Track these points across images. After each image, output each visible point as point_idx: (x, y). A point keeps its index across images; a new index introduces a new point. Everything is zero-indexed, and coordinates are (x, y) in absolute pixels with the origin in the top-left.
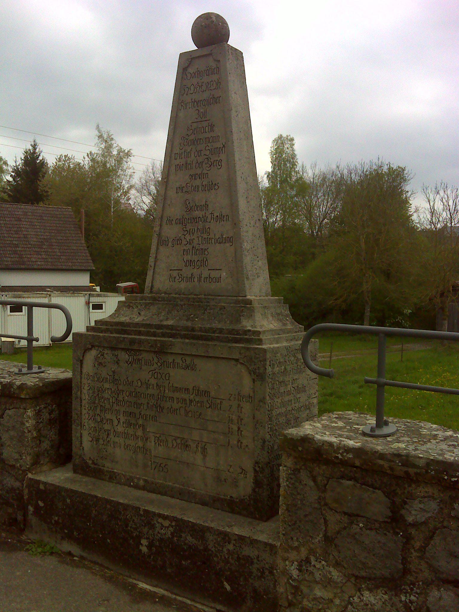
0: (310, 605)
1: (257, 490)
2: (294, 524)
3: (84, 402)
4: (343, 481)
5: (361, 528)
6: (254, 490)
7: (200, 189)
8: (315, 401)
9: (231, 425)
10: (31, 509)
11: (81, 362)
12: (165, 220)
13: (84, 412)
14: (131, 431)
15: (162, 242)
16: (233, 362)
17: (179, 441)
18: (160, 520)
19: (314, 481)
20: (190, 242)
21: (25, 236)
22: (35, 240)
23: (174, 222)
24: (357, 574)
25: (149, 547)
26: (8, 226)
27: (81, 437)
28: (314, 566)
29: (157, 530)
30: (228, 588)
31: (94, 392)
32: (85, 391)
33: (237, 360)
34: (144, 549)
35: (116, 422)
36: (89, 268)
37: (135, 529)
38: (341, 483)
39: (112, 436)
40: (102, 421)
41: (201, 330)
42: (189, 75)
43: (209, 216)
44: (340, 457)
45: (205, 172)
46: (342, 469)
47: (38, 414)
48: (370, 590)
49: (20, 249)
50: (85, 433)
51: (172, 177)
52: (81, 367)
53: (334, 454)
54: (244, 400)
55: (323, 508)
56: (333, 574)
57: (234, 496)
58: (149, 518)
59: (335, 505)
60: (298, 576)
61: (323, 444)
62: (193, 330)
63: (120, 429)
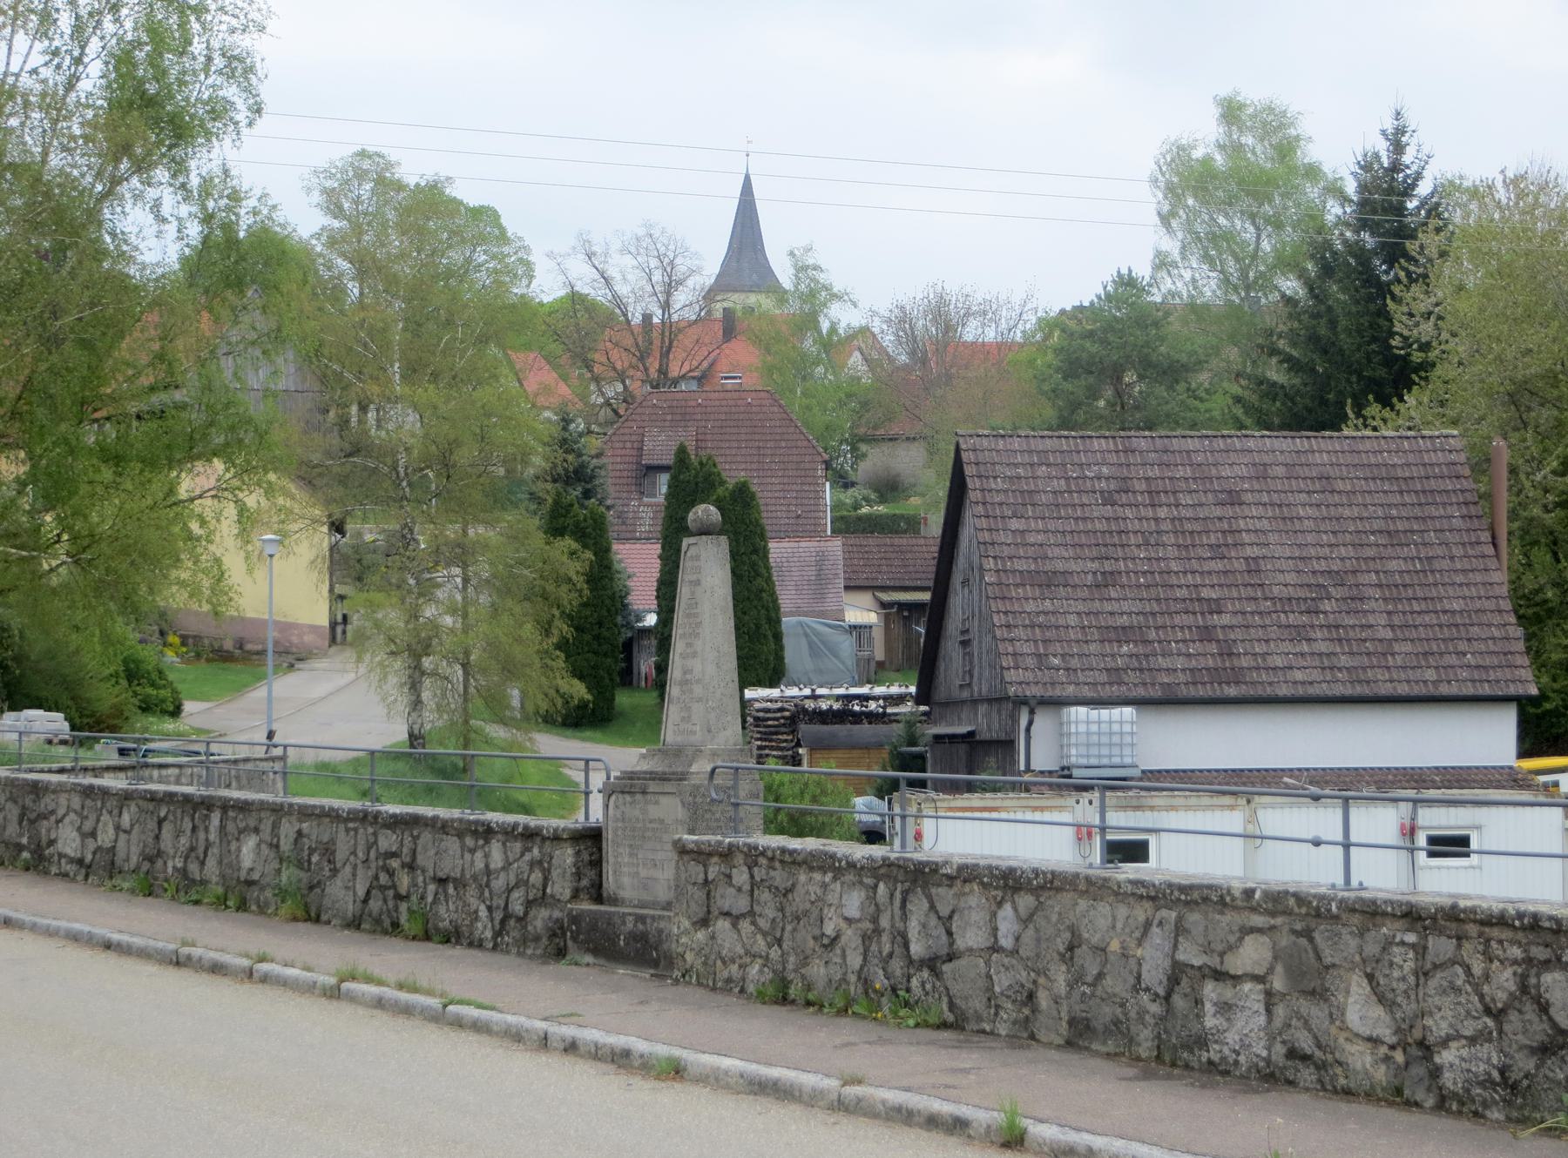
21: (1253, 566)
22: (1291, 578)
26: (1188, 526)
36: (1512, 690)
47: (578, 853)
49: (1226, 619)
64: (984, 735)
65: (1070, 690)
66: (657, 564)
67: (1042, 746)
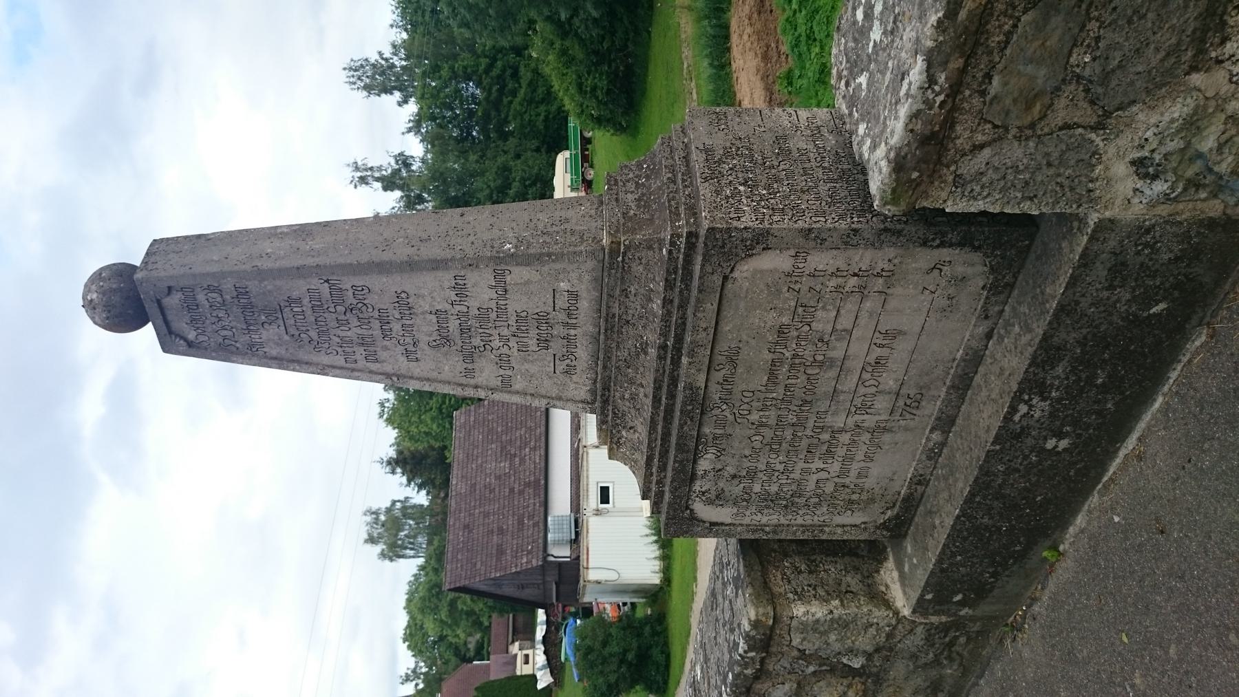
0: (1230, 159)
1: (976, 244)
2: (1062, 186)
3: (783, 521)
4: (993, 92)
5: (1094, 59)
6: (976, 249)
7: (408, 322)
8: (804, 114)
9: (847, 289)
10: (965, 611)
11: (713, 524)
12: (464, 380)
13: (800, 521)
14: (841, 451)
15: (506, 385)
16: (729, 285)
17: (866, 376)
18: (1017, 418)
19: (982, 147)
20: (505, 341)
23: (470, 366)
24: (1185, 67)
25: (1060, 435)
27: (844, 526)
28: (1153, 151)
29: (1032, 423)
30: (1162, 306)
31: (768, 507)
32: (764, 520)
33: (725, 278)
34: (1064, 444)
35: (823, 475)
37: (1026, 457)
38: (995, 97)
39: (847, 481)
40: (819, 496)
41: (664, 334)
42: (201, 338)
43: (458, 308)
44: (942, 97)
45: (376, 314)
46: (967, 93)
47: (801, 596)
48: (1223, 41)
49: (516, 486)
50: (839, 520)
51: (388, 368)
52: (722, 524)
53: (936, 109)
54: (801, 265)
55: (1039, 132)
56: (1176, 115)
57: (981, 284)
58: (1009, 435)
59: (1038, 107)
60: (1166, 181)
61: (912, 131)
62: (663, 347)
63: (835, 467)
64: (556, 578)
65: (541, 541)
66: (369, 214)
67: (561, 552)
